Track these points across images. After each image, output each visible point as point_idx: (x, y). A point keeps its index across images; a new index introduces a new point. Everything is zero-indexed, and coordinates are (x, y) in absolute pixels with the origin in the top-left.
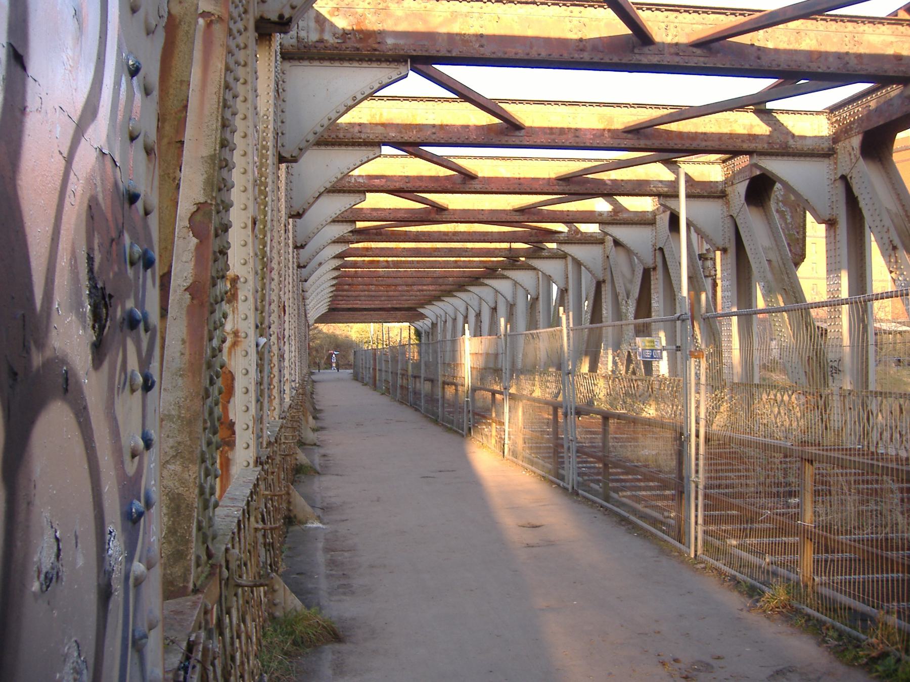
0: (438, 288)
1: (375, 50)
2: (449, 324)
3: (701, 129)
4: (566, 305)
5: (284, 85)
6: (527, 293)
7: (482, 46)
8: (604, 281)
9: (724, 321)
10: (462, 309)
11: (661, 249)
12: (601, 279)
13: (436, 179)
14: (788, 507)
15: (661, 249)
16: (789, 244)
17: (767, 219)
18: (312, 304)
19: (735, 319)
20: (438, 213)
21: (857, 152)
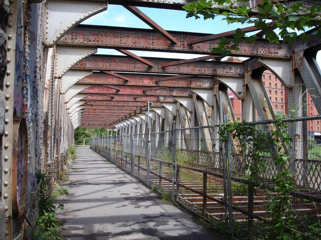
0: (117, 118)
1: (84, 68)
2: (123, 130)
3: (215, 56)
4: (176, 120)
5: (56, 64)
6: (152, 119)
7: (110, 67)
8: (165, 119)
9: (166, 133)
10: (127, 126)
11: (178, 110)
12: (176, 115)
13: (122, 49)
14: (303, 203)
15: (178, 110)
16: (208, 111)
17: (226, 95)
18: (73, 119)
19: (180, 131)
20: (131, 58)
21: (218, 89)
